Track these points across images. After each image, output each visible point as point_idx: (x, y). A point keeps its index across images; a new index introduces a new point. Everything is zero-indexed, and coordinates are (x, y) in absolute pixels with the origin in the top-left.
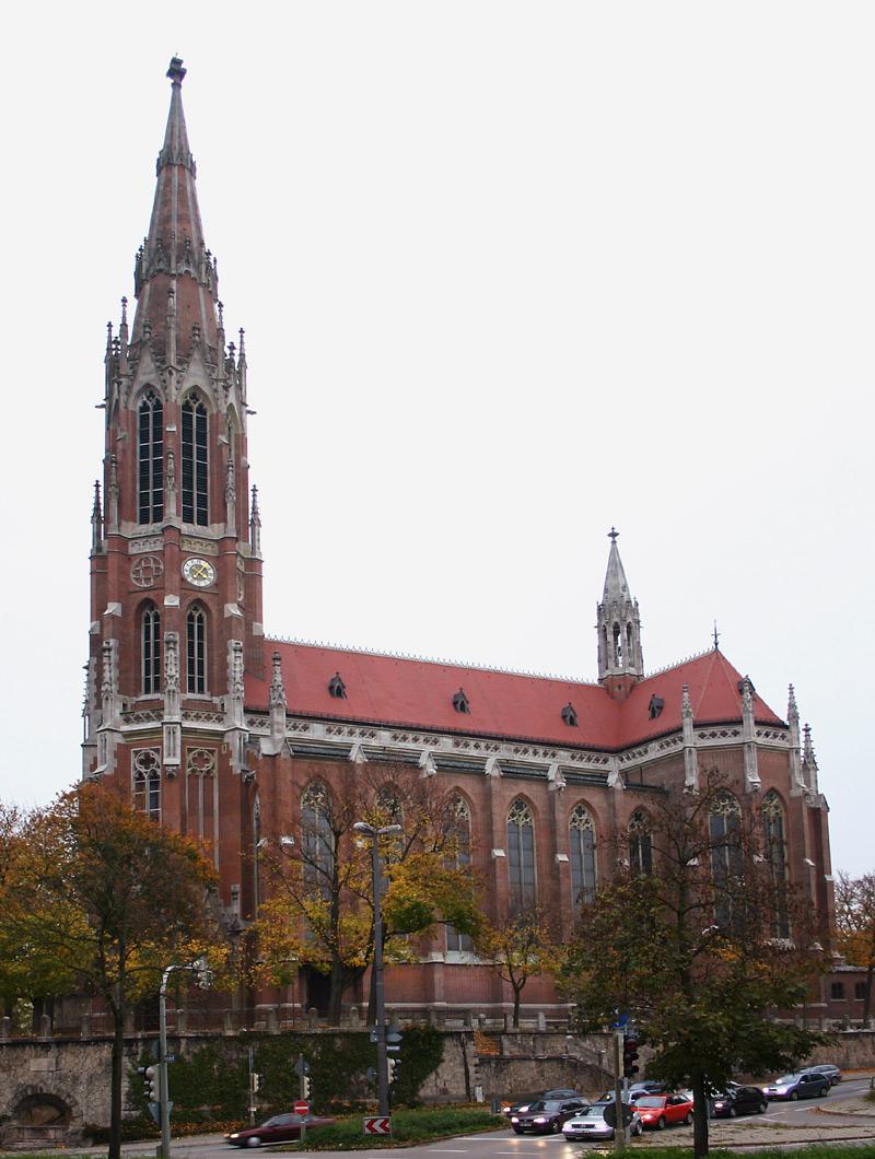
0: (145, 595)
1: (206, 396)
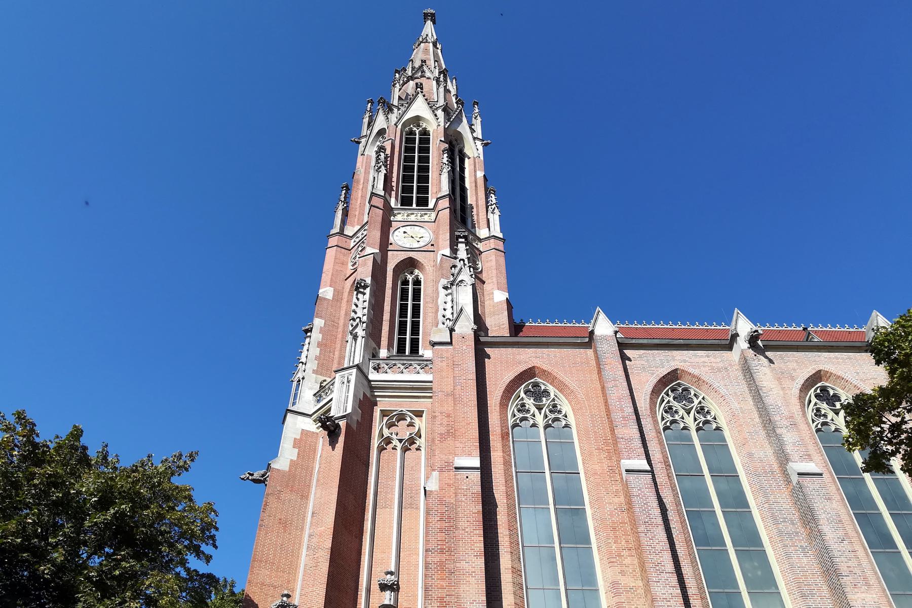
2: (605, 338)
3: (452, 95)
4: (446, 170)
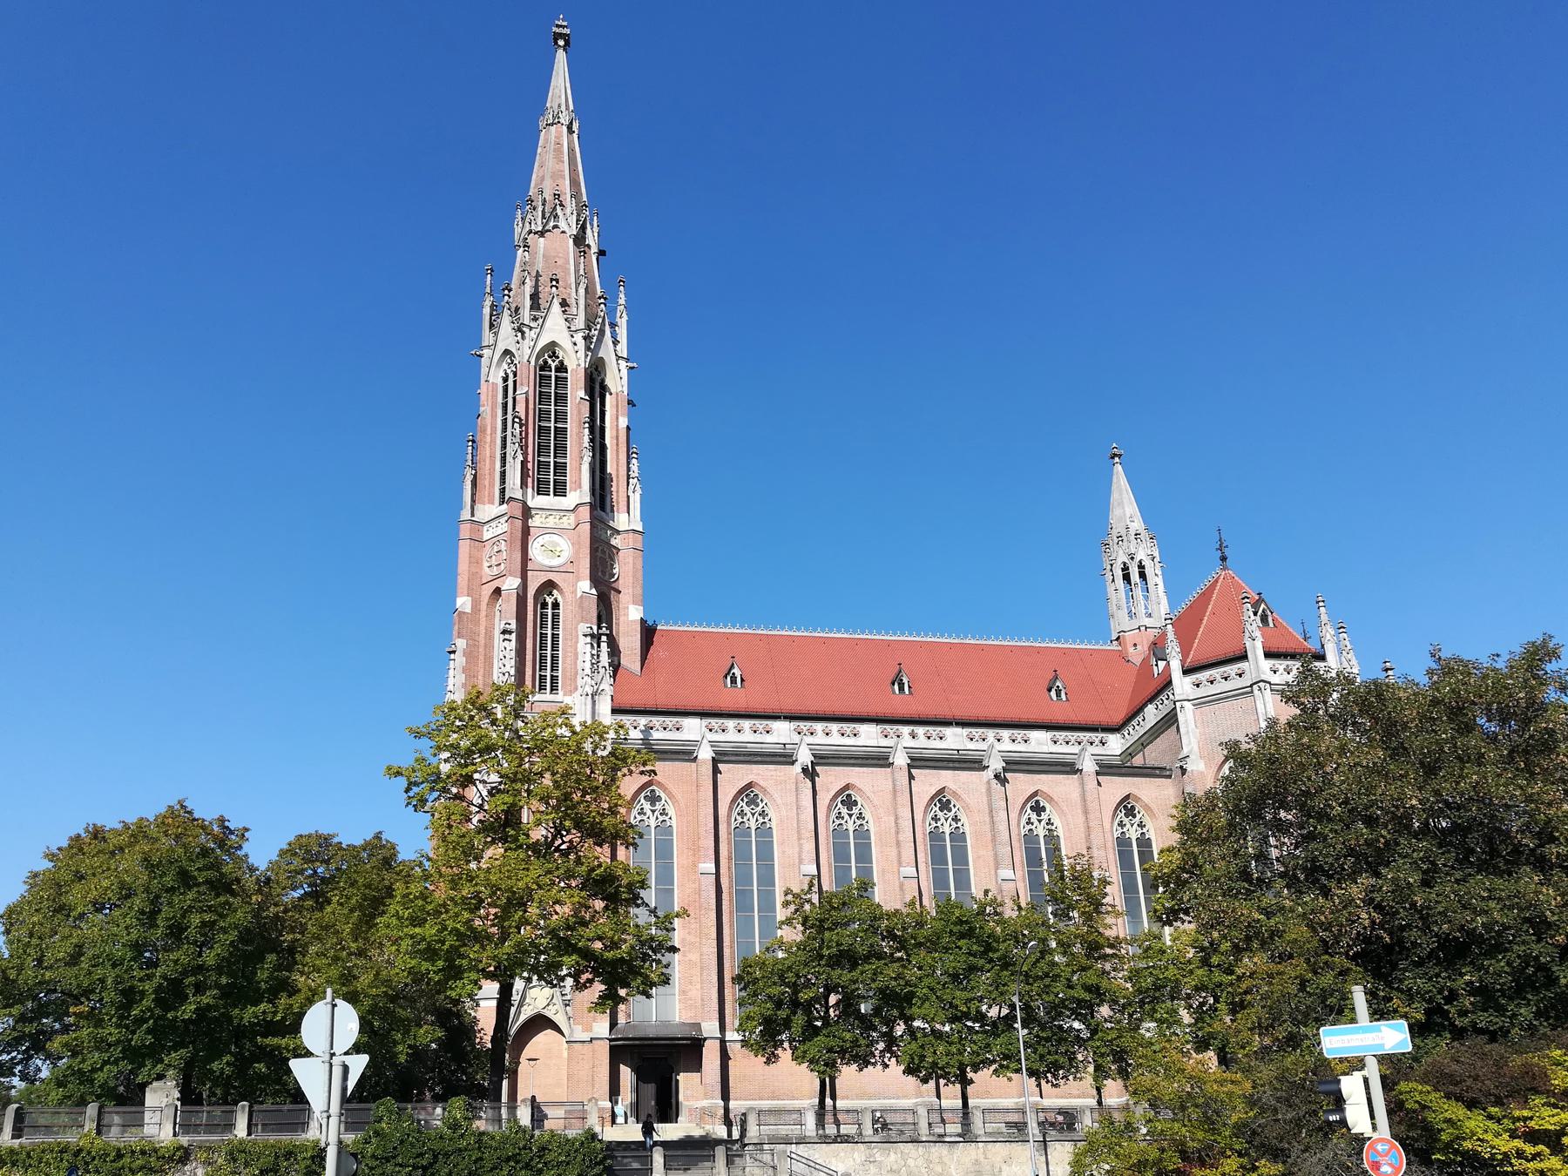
2: (704, 761)
3: (592, 251)
4: (587, 459)
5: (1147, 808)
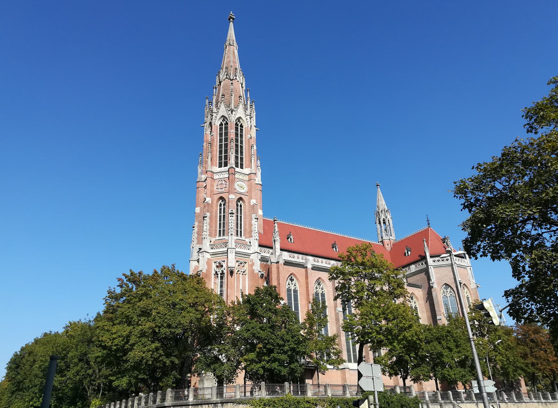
0: (221, 195)
1: (243, 121)
5: (416, 298)
